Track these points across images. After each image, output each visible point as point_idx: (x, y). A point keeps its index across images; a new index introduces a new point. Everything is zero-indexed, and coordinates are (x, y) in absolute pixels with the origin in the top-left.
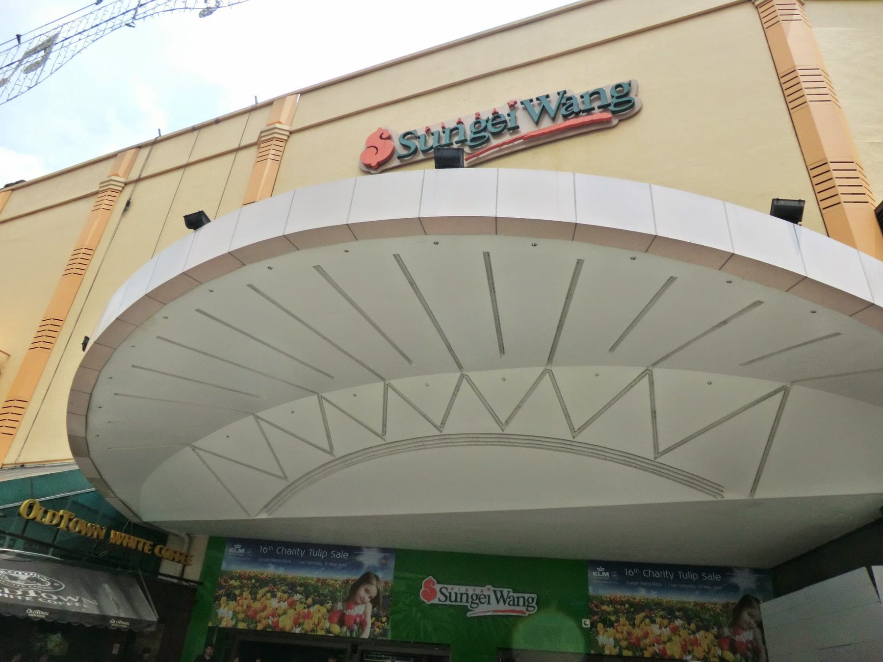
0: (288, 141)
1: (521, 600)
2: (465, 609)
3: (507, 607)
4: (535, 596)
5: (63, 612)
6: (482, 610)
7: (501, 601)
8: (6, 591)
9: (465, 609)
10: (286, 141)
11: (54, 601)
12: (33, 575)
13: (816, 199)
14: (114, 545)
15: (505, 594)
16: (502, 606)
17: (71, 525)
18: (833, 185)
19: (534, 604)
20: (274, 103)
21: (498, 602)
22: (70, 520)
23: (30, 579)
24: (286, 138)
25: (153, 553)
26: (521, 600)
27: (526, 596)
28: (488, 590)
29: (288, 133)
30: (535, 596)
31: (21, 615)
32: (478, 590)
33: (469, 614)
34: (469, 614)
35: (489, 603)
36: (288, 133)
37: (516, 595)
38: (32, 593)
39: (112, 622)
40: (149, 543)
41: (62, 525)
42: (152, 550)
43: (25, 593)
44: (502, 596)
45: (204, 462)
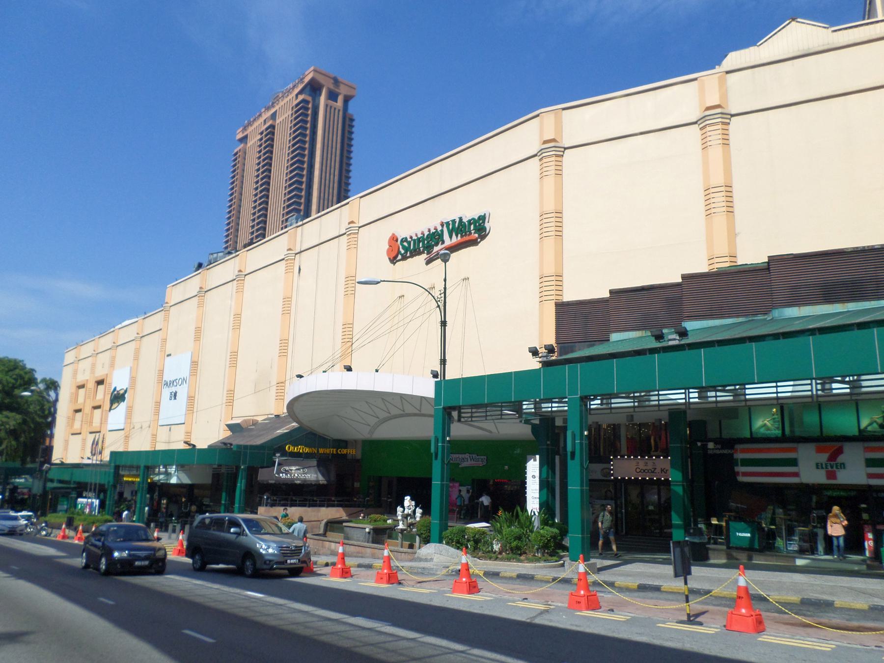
0: (564, 155)
1: (480, 459)
2: (459, 464)
3: (475, 463)
4: (485, 457)
5: (305, 480)
6: (465, 464)
7: (472, 460)
8: (289, 475)
9: (459, 464)
10: (358, 233)
11: (302, 477)
12: (297, 467)
13: (179, 304)
14: (321, 454)
15: (474, 457)
16: (473, 462)
17: (304, 450)
18: (834, 33)
19: (485, 461)
20: (698, 79)
21: (471, 460)
22: (303, 448)
23: (296, 469)
24: (357, 231)
25: (337, 453)
26: (480, 459)
27: (482, 457)
28: (467, 456)
29: (357, 228)
30: (485, 457)
31: (293, 483)
32: (463, 456)
33: (460, 466)
34: (460, 466)
35: (467, 461)
36: (357, 228)
37: (478, 457)
38: (296, 475)
39: (321, 482)
40: (335, 449)
41: (301, 451)
42: (337, 451)
43: (294, 475)
44: (473, 458)
45: (359, 415)
